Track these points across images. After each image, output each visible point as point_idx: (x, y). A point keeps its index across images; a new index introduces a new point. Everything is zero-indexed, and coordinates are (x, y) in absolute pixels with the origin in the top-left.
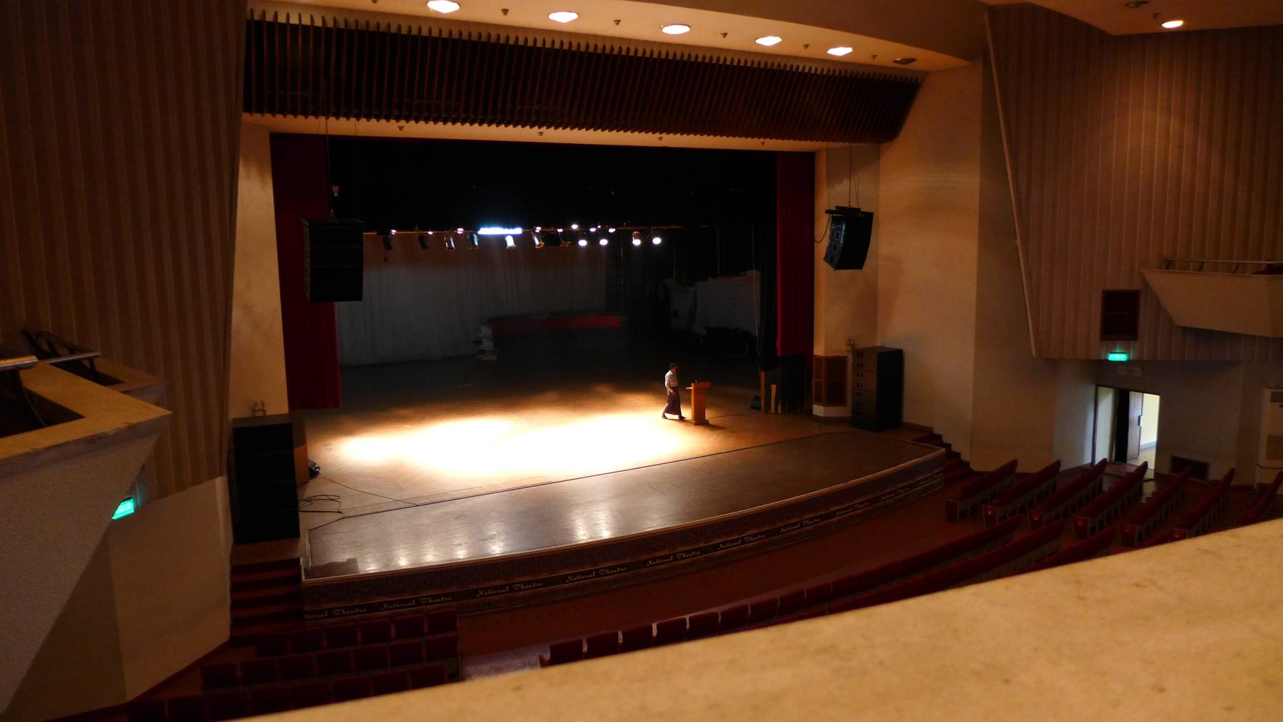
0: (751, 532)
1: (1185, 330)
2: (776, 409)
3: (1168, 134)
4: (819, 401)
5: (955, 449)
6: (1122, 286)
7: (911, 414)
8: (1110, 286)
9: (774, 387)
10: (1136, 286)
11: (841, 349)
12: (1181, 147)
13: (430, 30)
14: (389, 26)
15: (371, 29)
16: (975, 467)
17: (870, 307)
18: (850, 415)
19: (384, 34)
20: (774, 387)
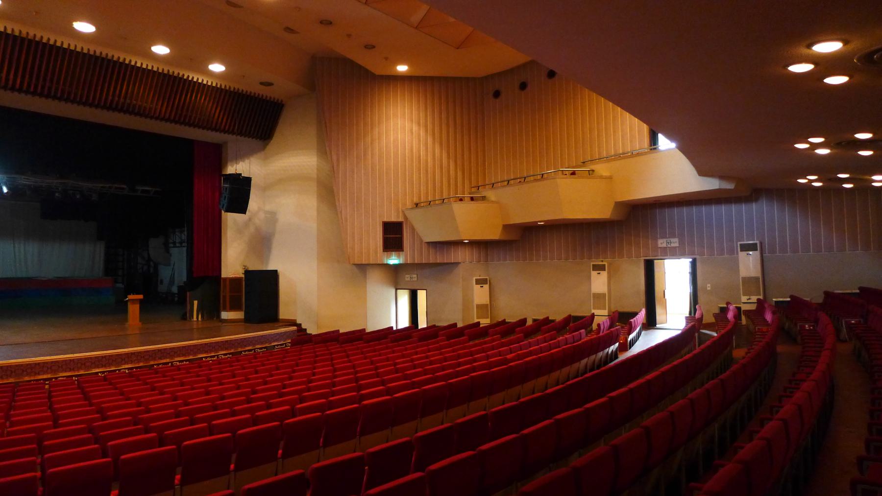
0: (127, 366)
1: (428, 243)
2: (197, 318)
3: (412, 133)
4: (225, 309)
5: (303, 327)
6: (393, 219)
7: (284, 313)
8: (385, 220)
9: (196, 302)
10: (401, 219)
11: (239, 273)
12: (419, 141)
13: (69, 45)
14: (42, 37)
15: (37, 39)
16: (308, 332)
17: (262, 242)
18: (243, 317)
19: (45, 45)
20: (196, 302)
